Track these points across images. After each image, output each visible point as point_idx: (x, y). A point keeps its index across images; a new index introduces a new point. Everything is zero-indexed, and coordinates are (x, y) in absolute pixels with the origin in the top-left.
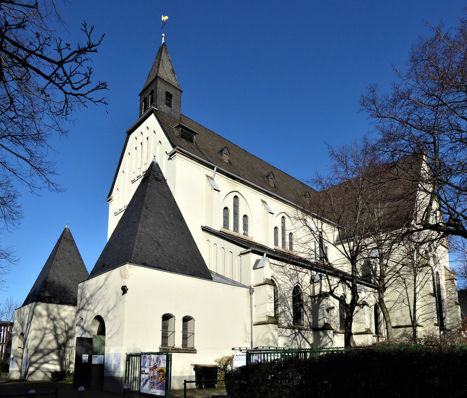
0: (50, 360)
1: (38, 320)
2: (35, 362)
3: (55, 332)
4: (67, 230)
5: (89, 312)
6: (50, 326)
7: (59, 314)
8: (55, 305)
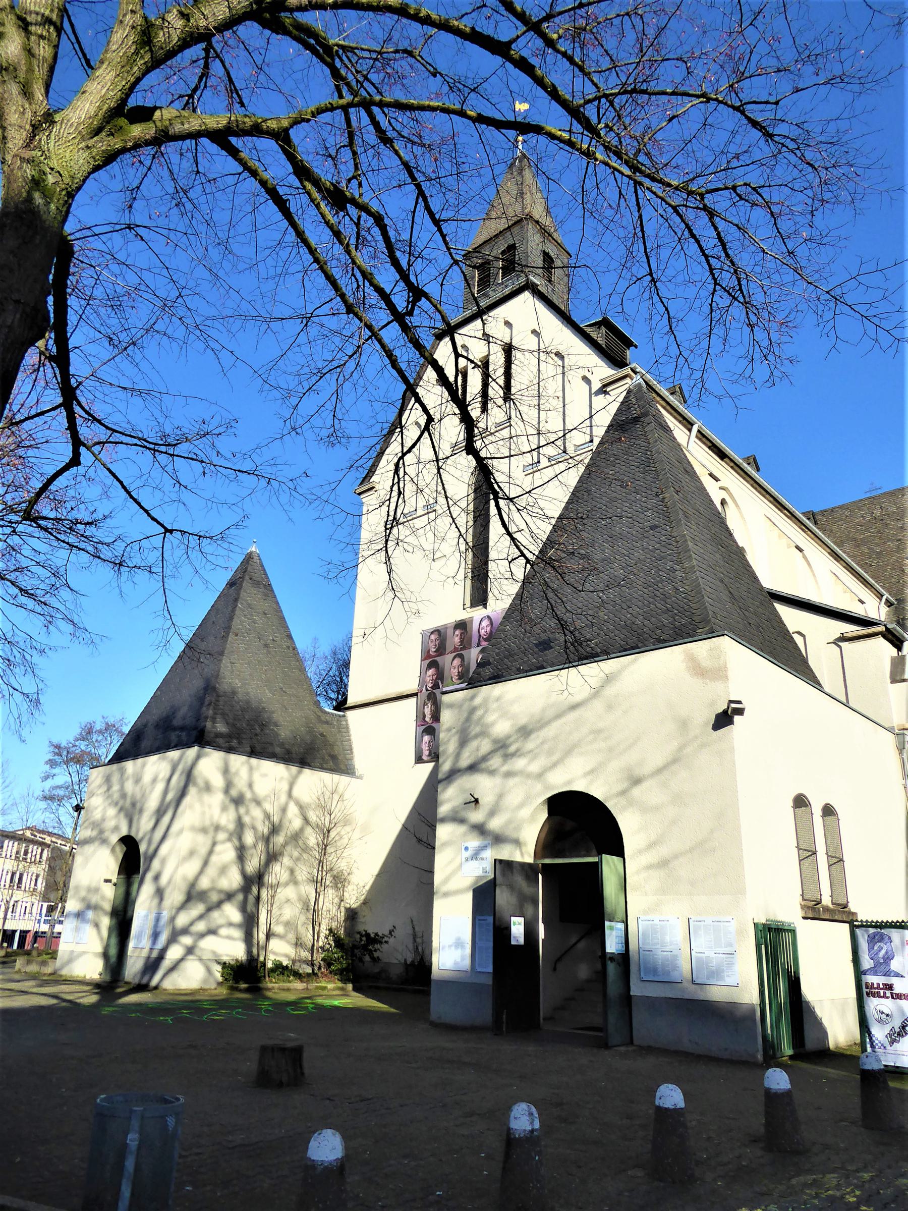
0: (221, 926)
1: (201, 800)
2: (185, 931)
3: (240, 839)
4: (256, 559)
5: (512, 782)
6: (228, 820)
7: (250, 786)
8: (244, 758)
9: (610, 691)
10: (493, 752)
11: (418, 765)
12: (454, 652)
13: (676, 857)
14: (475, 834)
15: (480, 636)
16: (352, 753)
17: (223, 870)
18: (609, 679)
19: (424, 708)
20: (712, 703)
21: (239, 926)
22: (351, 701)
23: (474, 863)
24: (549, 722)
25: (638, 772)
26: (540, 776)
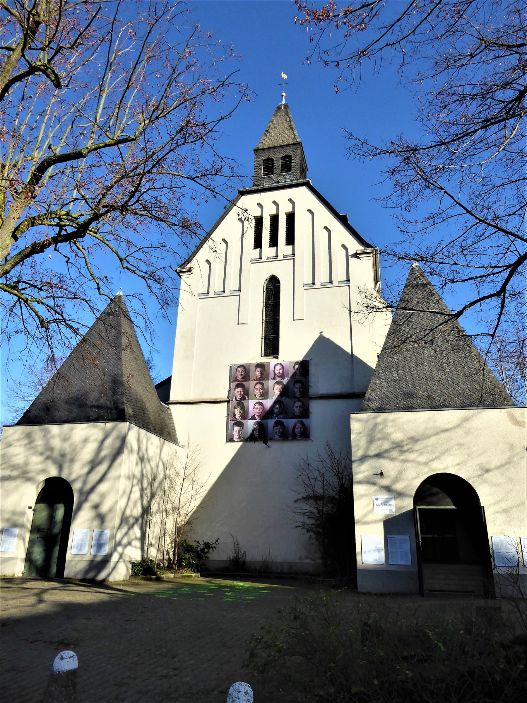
3: (142, 484)
5: (408, 465)
6: (137, 472)
9: (467, 425)
11: (229, 443)
12: (256, 380)
13: (511, 508)
14: (384, 491)
15: (275, 374)
16: (175, 431)
17: (135, 504)
18: (466, 420)
21: (139, 539)
22: (173, 398)
23: (384, 507)
24: (428, 437)
26: (426, 464)
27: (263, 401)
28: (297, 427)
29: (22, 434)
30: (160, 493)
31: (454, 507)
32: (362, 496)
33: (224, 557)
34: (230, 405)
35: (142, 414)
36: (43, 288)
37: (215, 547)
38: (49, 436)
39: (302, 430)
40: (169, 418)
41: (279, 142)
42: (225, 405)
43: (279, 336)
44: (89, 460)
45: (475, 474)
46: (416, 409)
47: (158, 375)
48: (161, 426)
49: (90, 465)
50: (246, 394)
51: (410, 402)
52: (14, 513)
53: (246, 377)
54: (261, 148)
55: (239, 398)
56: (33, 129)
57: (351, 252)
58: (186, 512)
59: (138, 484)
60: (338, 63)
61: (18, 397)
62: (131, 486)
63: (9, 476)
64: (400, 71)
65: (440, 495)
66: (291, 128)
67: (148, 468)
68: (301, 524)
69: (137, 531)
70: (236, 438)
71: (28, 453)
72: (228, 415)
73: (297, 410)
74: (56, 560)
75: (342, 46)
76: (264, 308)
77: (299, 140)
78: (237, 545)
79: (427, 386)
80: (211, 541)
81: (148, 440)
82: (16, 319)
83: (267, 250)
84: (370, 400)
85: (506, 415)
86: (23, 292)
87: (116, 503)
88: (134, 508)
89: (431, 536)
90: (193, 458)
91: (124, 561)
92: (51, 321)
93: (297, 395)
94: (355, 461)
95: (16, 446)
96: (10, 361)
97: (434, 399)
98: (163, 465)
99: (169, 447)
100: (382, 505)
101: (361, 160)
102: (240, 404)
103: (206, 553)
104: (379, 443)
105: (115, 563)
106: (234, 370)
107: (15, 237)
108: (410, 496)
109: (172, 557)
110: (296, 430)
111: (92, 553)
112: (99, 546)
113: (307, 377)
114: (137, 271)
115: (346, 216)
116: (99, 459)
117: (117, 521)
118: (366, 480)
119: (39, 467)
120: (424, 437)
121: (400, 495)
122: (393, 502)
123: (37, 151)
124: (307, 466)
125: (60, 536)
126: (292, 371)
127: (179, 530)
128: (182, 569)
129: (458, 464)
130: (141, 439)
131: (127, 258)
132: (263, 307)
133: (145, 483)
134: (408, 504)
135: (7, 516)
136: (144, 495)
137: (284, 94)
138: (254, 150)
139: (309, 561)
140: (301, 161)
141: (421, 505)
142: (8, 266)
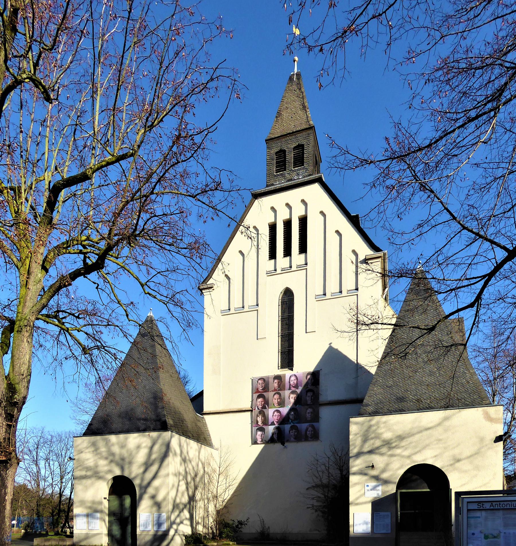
3: (186, 480)
6: (182, 470)
9: (447, 423)
10: (383, 446)
14: (373, 480)
15: (290, 385)
17: (183, 495)
18: (446, 419)
19: (257, 418)
20: (495, 432)
21: (189, 519)
23: (373, 492)
24: (413, 435)
25: (459, 457)
26: (409, 457)
27: (281, 409)
28: (309, 430)
29: (89, 443)
30: (201, 486)
31: (429, 490)
32: (356, 484)
33: (254, 531)
34: (253, 414)
35: (182, 425)
36: (80, 316)
37: (246, 524)
38: (110, 444)
39: (313, 432)
40: (204, 426)
41: (292, 128)
42: (249, 413)
43: (293, 349)
44: (143, 462)
45: (448, 463)
46: (405, 411)
47: (194, 388)
48: (197, 433)
49: (145, 466)
50: (266, 404)
51: (401, 405)
52: (93, 502)
53: (266, 389)
54: (273, 137)
55: (260, 407)
56: (38, 143)
57: (361, 258)
58: (222, 499)
59: (183, 480)
60: (322, 48)
61: (82, 412)
62: (178, 481)
63: (85, 475)
64: (388, 51)
65: (419, 481)
66: (304, 107)
67: (190, 466)
68: (311, 506)
69: (186, 514)
70: (259, 440)
71: (96, 458)
72: (252, 422)
73: (308, 416)
74: (130, 535)
75: (318, 32)
76: (280, 322)
77: (311, 122)
78: (263, 522)
79: (417, 391)
80: (243, 519)
81: (187, 445)
82: (64, 347)
83: (282, 261)
84: (367, 405)
85: (482, 413)
86: (64, 320)
87: (168, 494)
88: (182, 497)
89: (413, 511)
90: (225, 458)
91: (179, 535)
92: (91, 348)
93: (309, 402)
94: (352, 457)
95: (86, 453)
96: (66, 384)
97: (422, 402)
98: (202, 464)
99: (205, 450)
100: (371, 490)
101: (342, 174)
102: (262, 413)
103: (240, 528)
104: (372, 442)
105: (172, 536)
106: (255, 382)
107: (45, 269)
108: (395, 483)
109: (215, 531)
110: (308, 432)
111: (155, 530)
112: (159, 525)
113: (318, 386)
114: (158, 297)
115: (357, 216)
116: (151, 461)
117: (170, 507)
118: (360, 471)
119: (106, 468)
120: (410, 435)
121: (386, 482)
122: (380, 488)
123: (46, 172)
124: (316, 462)
125: (130, 518)
126: (304, 381)
127: (218, 512)
128: (223, 539)
129: (435, 456)
130: (182, 445)
131: (148, 283)
132: (279, 321)
133: (189, 479)
134: (392, 489)
135: (89, 505)
136: (189, 488)
137: (296, 58)
138: (266, 140)
139: (317, 532)
140: (314, 151)
141: (403, 489)
142: (44, 300)
